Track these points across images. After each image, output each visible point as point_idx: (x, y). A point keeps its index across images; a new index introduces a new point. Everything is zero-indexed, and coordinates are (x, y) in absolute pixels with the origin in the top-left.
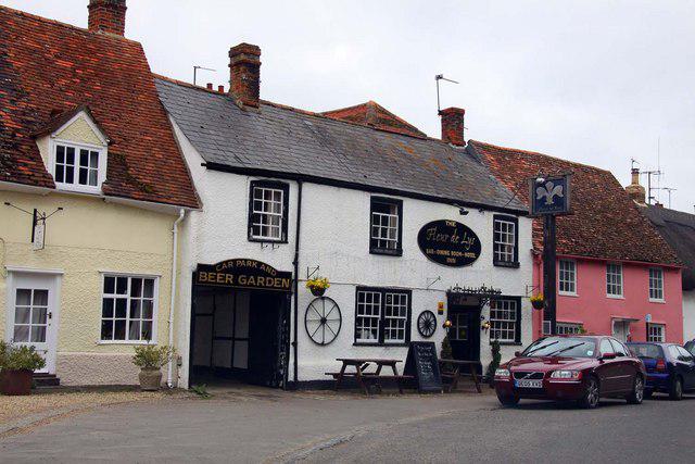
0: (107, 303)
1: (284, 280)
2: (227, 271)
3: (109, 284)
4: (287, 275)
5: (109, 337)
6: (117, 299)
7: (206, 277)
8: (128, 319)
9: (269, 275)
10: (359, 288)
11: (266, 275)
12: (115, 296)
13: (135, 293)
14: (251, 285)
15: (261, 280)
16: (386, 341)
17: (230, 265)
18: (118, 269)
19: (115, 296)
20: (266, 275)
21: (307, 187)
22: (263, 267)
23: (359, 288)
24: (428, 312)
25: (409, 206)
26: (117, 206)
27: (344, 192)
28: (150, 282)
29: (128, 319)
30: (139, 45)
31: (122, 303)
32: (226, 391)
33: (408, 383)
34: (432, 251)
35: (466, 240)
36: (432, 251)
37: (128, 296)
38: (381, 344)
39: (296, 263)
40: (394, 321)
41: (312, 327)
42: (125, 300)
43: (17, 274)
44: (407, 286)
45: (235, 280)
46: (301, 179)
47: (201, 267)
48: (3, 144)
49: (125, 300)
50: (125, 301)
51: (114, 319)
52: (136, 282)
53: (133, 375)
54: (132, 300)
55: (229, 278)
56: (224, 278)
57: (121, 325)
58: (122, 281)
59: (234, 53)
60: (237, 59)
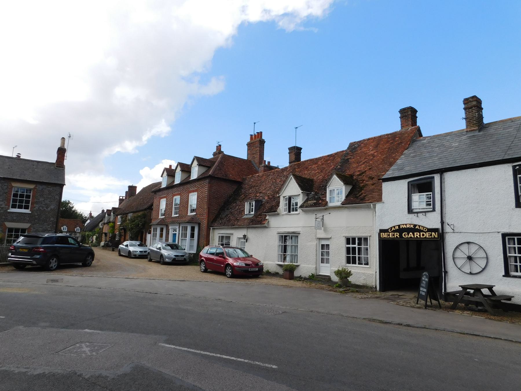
0: (348, 249)
1: (433, 233)
3: (348, 241)
4: (435, 230)
5: (350, 263)
7: (384, 235)
8: (357, 256)
9: (423, 231)
10: (504, 236)
11: (420, 231)
12: (351, 246)
13: (359, 244)
14: (411, 237)
15: (417, 234)
17: (393, 229)
18: (351, 235)
19: (351, 246)
20: (420, 231)
21: (449, 176)
22: (417, 227)
23: (504, 236)
26: (346, 207)
28: (366, 239)
29: (357, 256)
31: (354, 249)
33: (176, 262)
37: (356, 246)
39: (442, 223)
41: (460, 263)
42: (355, 247)
43: (320, 239)
45: (401, 235)
46: (442, 171)
47: (381, 231)
49: (355, 247)
50: (355, 249)
51: (351, 255)
52: (360, 239)
53: (127, 255)
55: (397, 235)
56: (394, 235)
57: (354, 258)
58: (354, 239)
59: (466, 101)
60: (470, 104)
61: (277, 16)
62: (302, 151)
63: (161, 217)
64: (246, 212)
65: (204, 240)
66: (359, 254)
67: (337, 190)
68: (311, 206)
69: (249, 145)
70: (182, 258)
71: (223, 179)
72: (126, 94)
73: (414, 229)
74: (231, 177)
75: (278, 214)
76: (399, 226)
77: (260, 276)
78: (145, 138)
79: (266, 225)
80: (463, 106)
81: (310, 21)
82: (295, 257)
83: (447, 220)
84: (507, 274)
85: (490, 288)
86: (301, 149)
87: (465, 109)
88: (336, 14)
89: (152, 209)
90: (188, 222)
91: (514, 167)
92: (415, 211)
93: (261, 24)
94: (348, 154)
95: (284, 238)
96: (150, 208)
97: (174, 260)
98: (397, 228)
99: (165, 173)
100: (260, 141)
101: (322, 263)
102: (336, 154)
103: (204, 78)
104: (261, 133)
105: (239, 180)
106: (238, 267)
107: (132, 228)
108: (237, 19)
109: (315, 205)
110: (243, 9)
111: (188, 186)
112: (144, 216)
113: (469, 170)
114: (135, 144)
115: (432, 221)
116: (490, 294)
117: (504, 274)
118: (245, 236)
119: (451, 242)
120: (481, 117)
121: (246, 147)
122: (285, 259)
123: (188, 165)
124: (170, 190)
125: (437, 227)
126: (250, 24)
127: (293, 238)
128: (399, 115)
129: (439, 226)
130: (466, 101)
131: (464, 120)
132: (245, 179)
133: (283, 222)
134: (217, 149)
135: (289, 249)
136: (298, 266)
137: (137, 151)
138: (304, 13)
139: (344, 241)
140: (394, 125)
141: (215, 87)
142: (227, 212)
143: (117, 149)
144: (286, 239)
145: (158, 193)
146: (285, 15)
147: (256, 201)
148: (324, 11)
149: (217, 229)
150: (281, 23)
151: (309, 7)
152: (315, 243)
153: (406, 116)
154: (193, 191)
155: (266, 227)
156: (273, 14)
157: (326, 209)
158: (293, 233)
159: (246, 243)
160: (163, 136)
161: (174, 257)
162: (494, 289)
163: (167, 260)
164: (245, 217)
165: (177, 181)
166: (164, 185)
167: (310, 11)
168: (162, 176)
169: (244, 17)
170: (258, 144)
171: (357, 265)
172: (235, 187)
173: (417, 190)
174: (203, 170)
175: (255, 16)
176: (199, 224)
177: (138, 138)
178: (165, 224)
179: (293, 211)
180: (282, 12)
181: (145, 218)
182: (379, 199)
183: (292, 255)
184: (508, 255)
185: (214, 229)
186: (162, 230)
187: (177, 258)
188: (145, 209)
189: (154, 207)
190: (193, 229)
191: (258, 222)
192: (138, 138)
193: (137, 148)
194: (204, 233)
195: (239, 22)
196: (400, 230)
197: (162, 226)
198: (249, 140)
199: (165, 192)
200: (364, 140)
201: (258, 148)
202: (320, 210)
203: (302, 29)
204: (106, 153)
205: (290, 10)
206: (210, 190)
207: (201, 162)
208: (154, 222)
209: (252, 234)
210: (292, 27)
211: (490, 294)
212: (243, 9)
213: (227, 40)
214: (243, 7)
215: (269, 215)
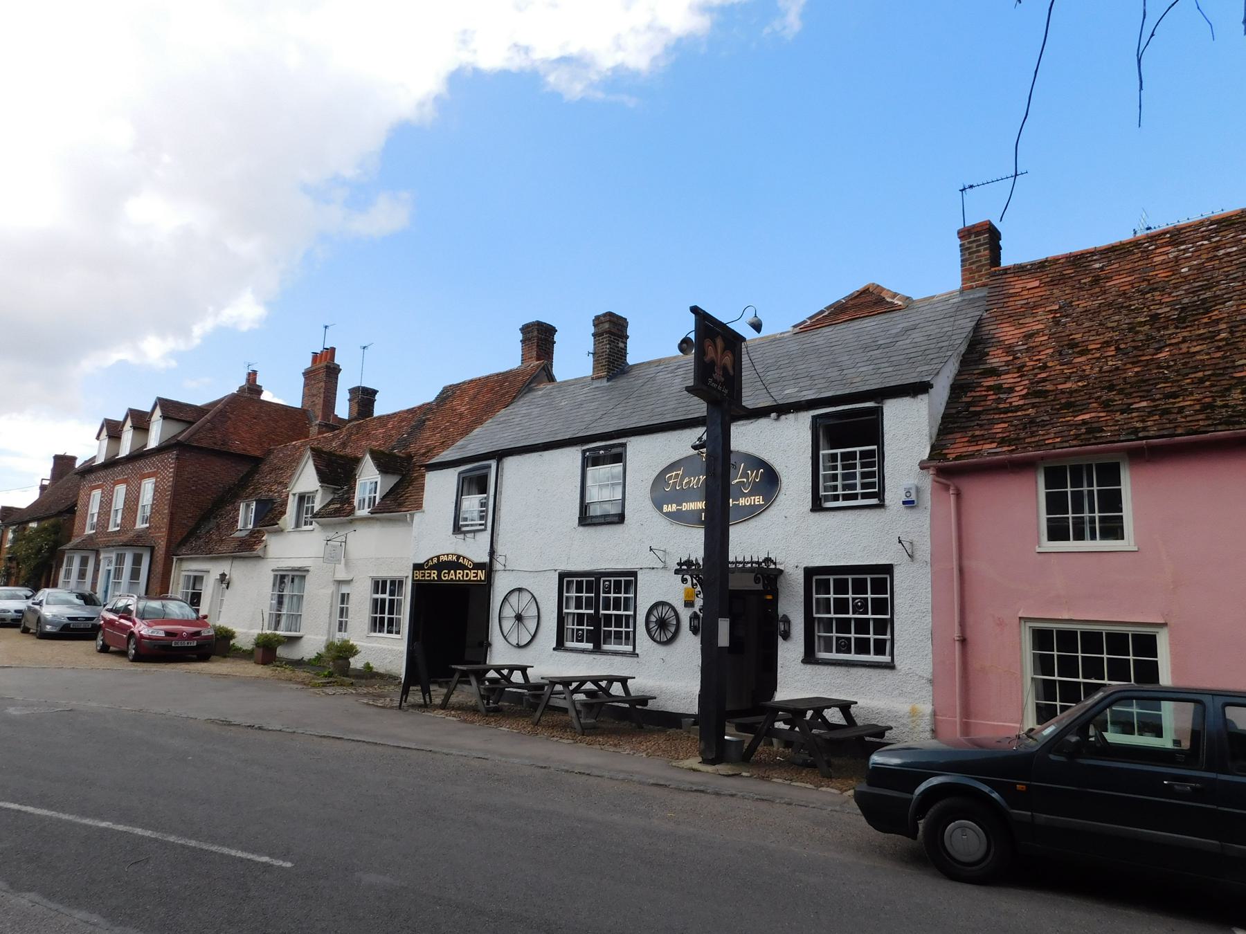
2: (432, 568)
4: (478, 566)
6: (869, 653)
16: (569, 644)
21: (510, 463)
24: (663, 604)
25: (635, 447)
26: (378, 519)
27: (547, 454)
30: (610, 314)
32: (1133, 913)
34: (673, 508)
35: (745, 475)
36: (673, 508)
38: (597, 650)
39: (492, 553)
40: (618, 617)
41: (507, 625)
44: (628, 566)
45: (439, 576)
46: (500, 455)
48: (1241, 345)
54: (856, 653)
55: (434, 574)
61: (544, 61)
62: (377, 397)
63: (89, 531)
64: (240, 525)
65: (159, 587)
66: (391, 612)
67: (370, 481)
68: (330, 515)
69: (308, 374)
70: (89, 624)
71: (213, 450)
72: (158, 217)
73: (456, 565)
74: (237, 445)
75: (282, 531)
76: (438, 557)
77: (213, 657)
78: (197, 331)
79: (261, 554)
80: (592, 330)
81: (619, 80)
82: (296, 619)
83: (500, 549)
84: (560, 645)
85: (845, 707)
86: (375, 392)
87: (594, 335)
88: (688, 67)
89: (74, 512)
90: (126, 545)
91: (584, 452)
92: (464, 529)
93: (504, 76)
94: (431, 409)
95: (281, 579)
96: (71, 510)
97: (65, 627)
98: (435, 561)
99: (105, 432)
100: (327, 367)
101: (340, 630)
102: (420, 407)
103: (359, 195)
104: (333, 349)
105: (258, 453)
106: (150, 638)
107: (28, 557)
108: (447, 59)
109: (336, 513)
110: (465, 39)
111: (141, 463)
112: (57, 529)
113: (527, 456)
114: (171, 344)
115: (475, 549)
116: (843, 722)
117: (554, 645)
118: (223, 576)
119: (502, 585)
120: (623, 353)
121: (302, 379)
122: (278, 623)
123: (145, 413)
124: (110, 471)
125: (482, 561)
126: (477, 72)
127: (296, 581)
128: (520, 336)
129: (486, 559)
130: (526, 329)
131: (232, 385)
132: (269, 452)
133: (295, 546)
134: (248, 380)
135: (286, 600)
136: (299, 638)
137: (173, 363)
138: (607, 61)
139: (369, 585)
140: (508, 356)
141: (387, 217)
142: (212, 524)
143: (119, 355)
144: (288, 581)
145: (88, 477)
146: (565, 60)
147: (258, 502)
148: (654, 59)
149: (187, 559)
150: (551, 79)
151: (619, 47)
152: (331, 589)
153: (530, 340)
154: (149, 476)
155: (259, 557)
156: (537, 55)
157: (351, 522)
158: (299, 570)
159: (227, 592)
160: (244, 328)
161: (66, 621)
162: (853, 709)
163: (48, 628)
164: (237, 534)
165: (125, 449)
166: (100, 460)
167: (619, 57)
168: (98, 438)
169: (465, 57)
170: (322, 376)
171: (385, 635)
172: (244, 469)
173: (474, 488)
174: (175, 428)
175: (492, 56)
176: (152, 550)
177: (183, 330)
178: (92, 547)
179: (306, 524)
180: (555, 54)
181: (56, 533)
182: (418, 506)
183: (289, 616)
184: (565, 611)
185: (181, 560)
186: (84, 562)
187: (73, 624)
188: (60, 513)
189: (79, 508)
190: (137, 560)
191: (248, 548)
192: (183, 330)
193: (173, 354)
194: (159, 569)
195: (453, 67)
196: (441, 565)
197: (85, 554)
198: (308, 364)
199: (102, 474)
200: (464, 383)
201: (323, 384)
202: (342, 524)
203: (600, 95)
204: (89, 365)
205: (573, 50)
206: (178, 474)
207: (170, 409)
208: (75, 541)
209: (235, 571)
210: (576, 90)
211: (843, 722)
212: (465, 39)
213: (421, 104)
214: (465, 32)
215: (269, 532)
